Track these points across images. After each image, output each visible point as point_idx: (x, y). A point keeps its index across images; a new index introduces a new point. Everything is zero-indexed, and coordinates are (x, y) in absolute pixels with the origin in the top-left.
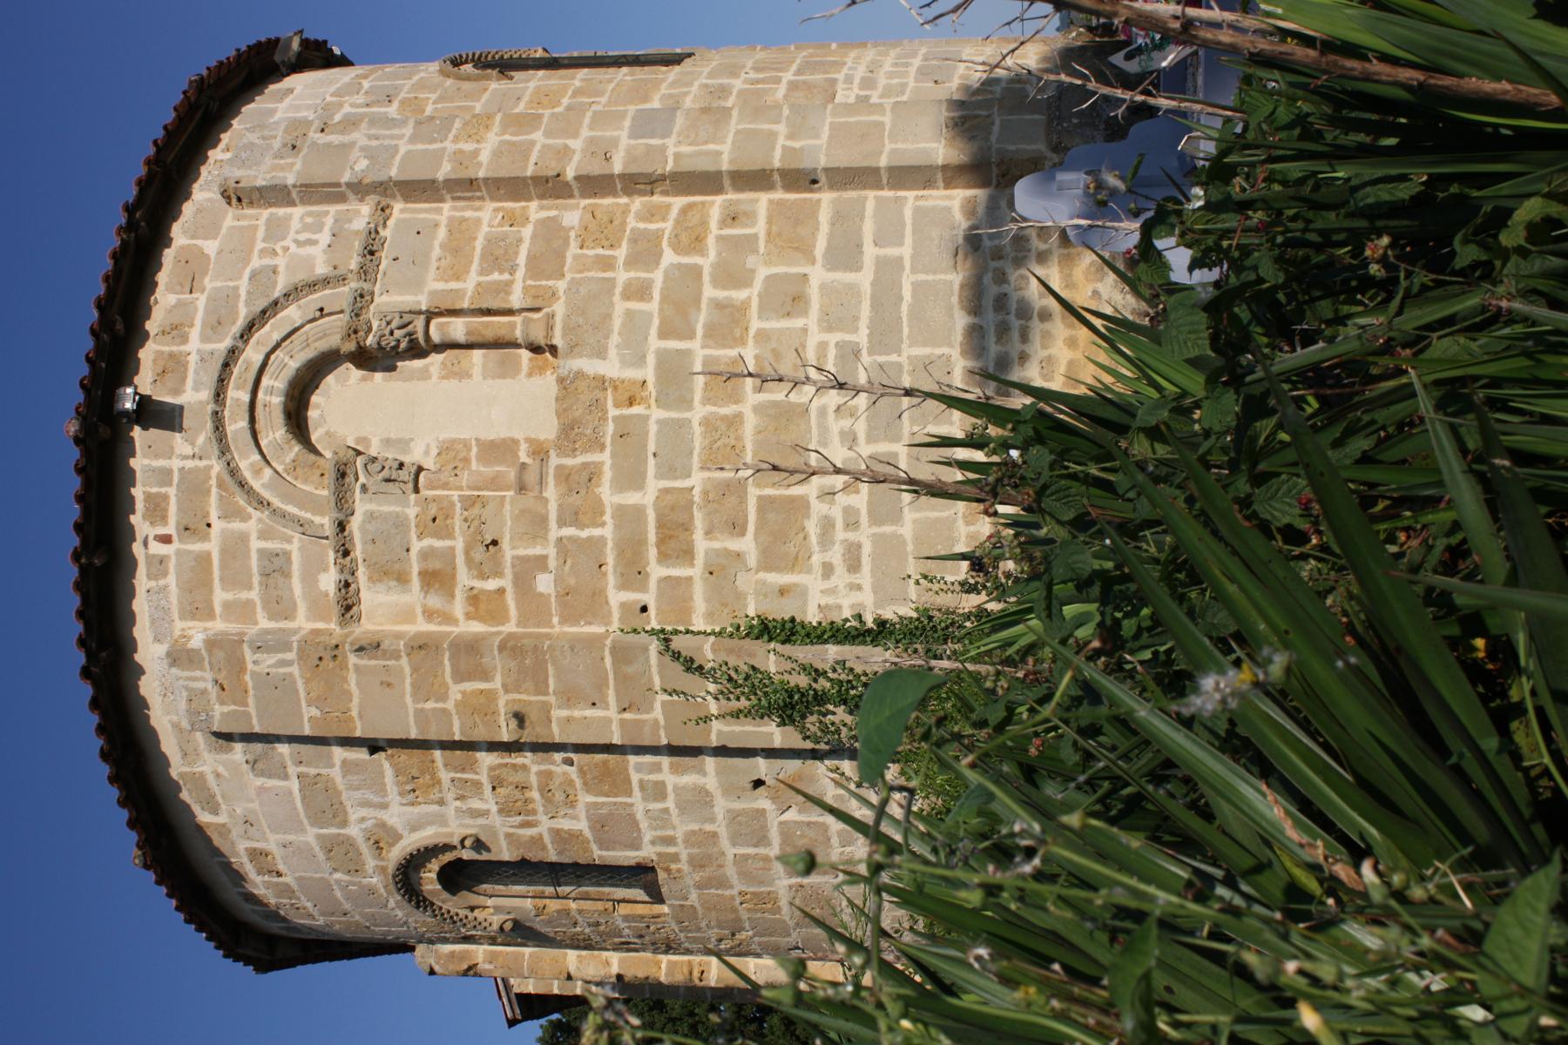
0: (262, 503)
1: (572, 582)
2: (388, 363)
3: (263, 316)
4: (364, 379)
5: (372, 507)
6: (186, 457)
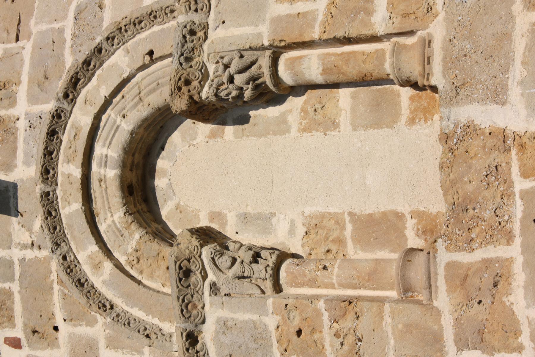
0: (106, 307)
2: (238, 112)
3: (88, 66)
4: (213, 135)
5: (225, 314)
6: (24, 247)
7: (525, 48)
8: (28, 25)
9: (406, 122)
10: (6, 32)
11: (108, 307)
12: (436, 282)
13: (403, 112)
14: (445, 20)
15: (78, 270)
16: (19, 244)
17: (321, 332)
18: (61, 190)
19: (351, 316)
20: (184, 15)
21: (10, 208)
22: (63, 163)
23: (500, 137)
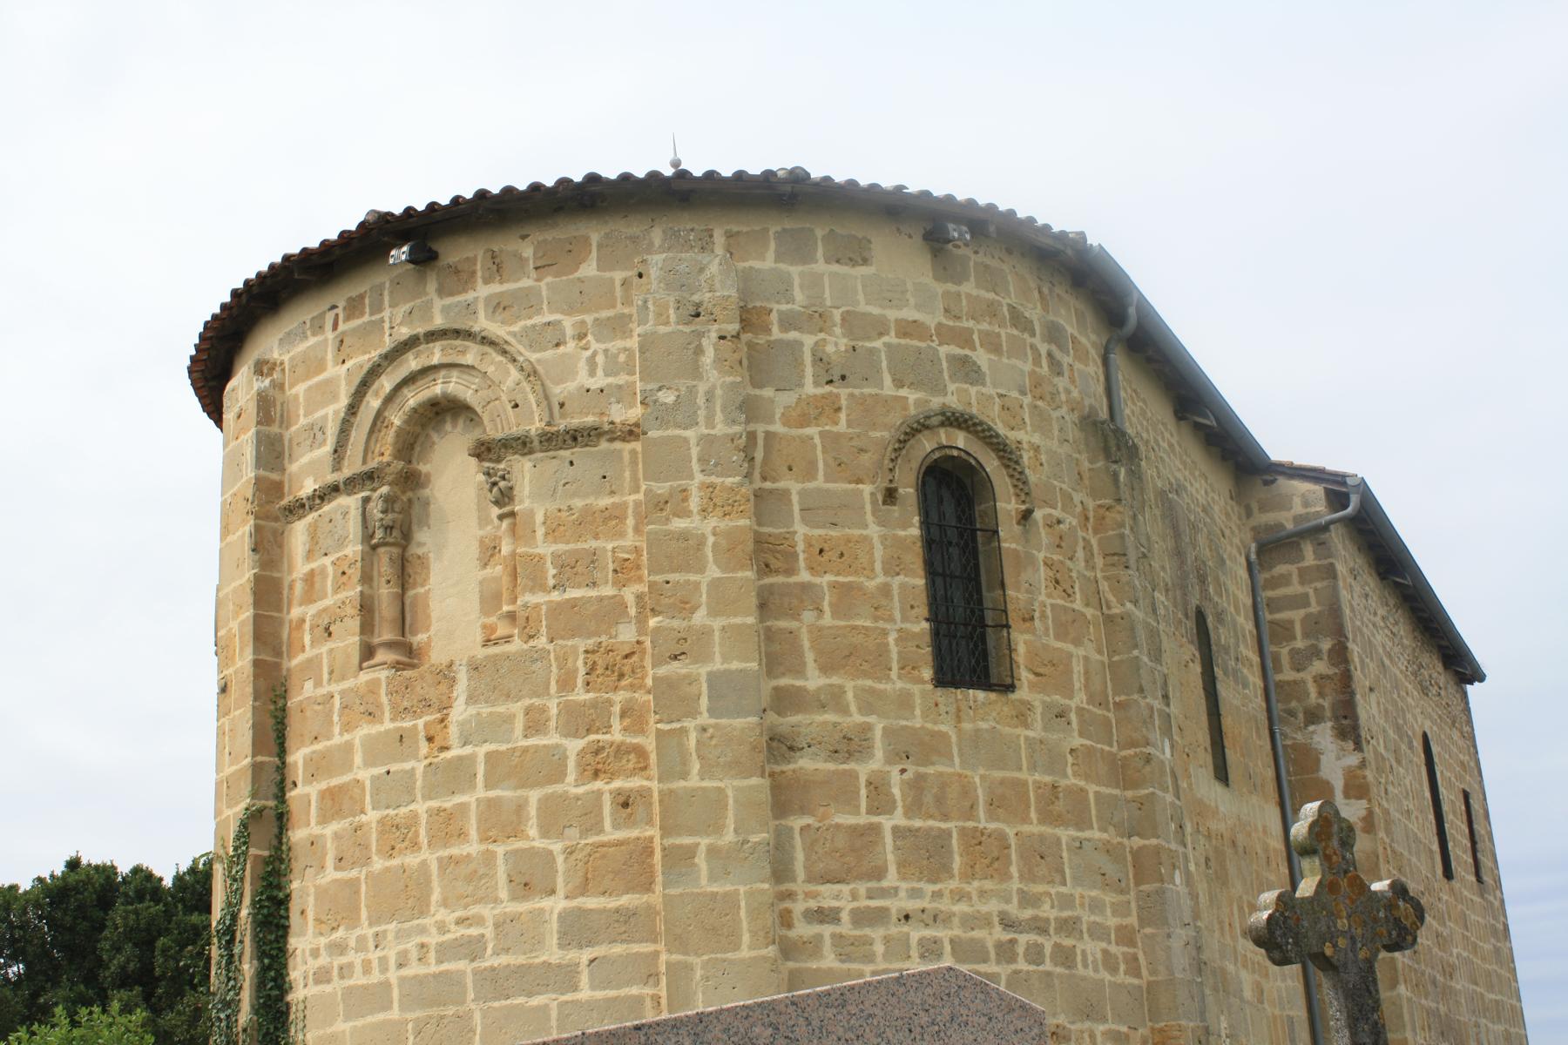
1: (308, 714)
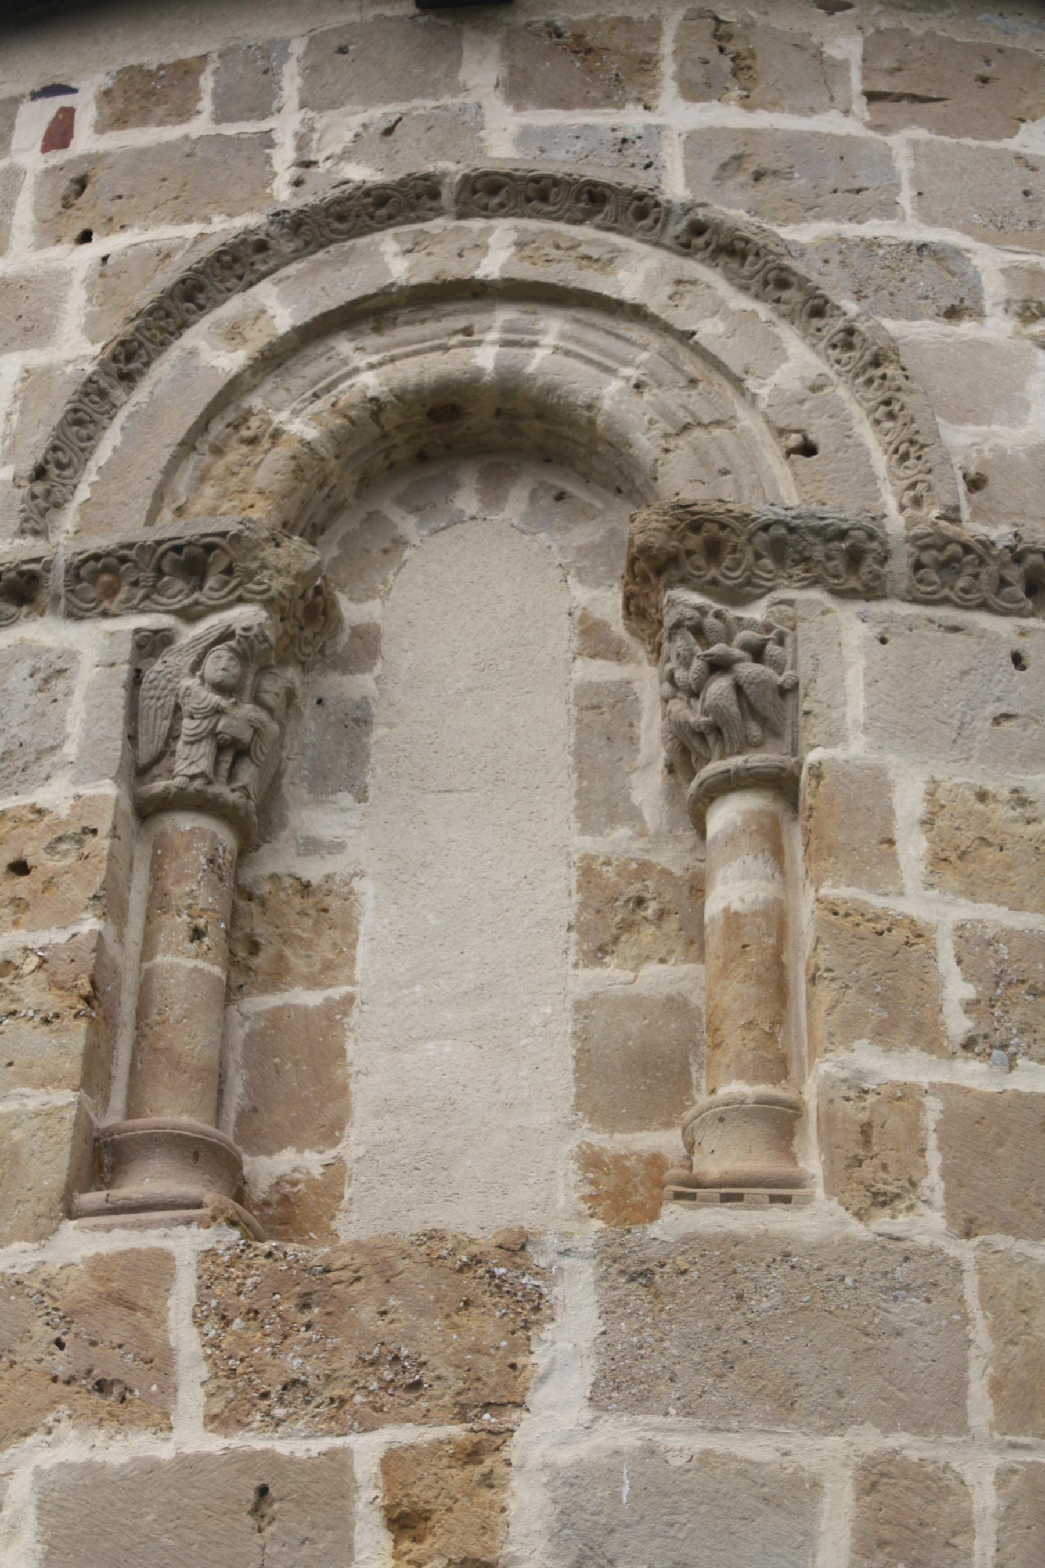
0: (127, 361)
3: (775, 279)
5: (86, 673)
6: (302, 142)
7: (749, 1462)
8: (913, 121)
9: (589, 1145)
10: (896, 65)
11: (126, 369)
12: (124, 1226)
13: (618, 1136)
14: (847, 1240)
15: (229, 285)
16: (312, 130)
17: (16, 923)
18: (445, 229)
19: (51, 1001)
20: (905, 533)
21: (408, 99)
22: (516, 229)
23: (502, 1391)
